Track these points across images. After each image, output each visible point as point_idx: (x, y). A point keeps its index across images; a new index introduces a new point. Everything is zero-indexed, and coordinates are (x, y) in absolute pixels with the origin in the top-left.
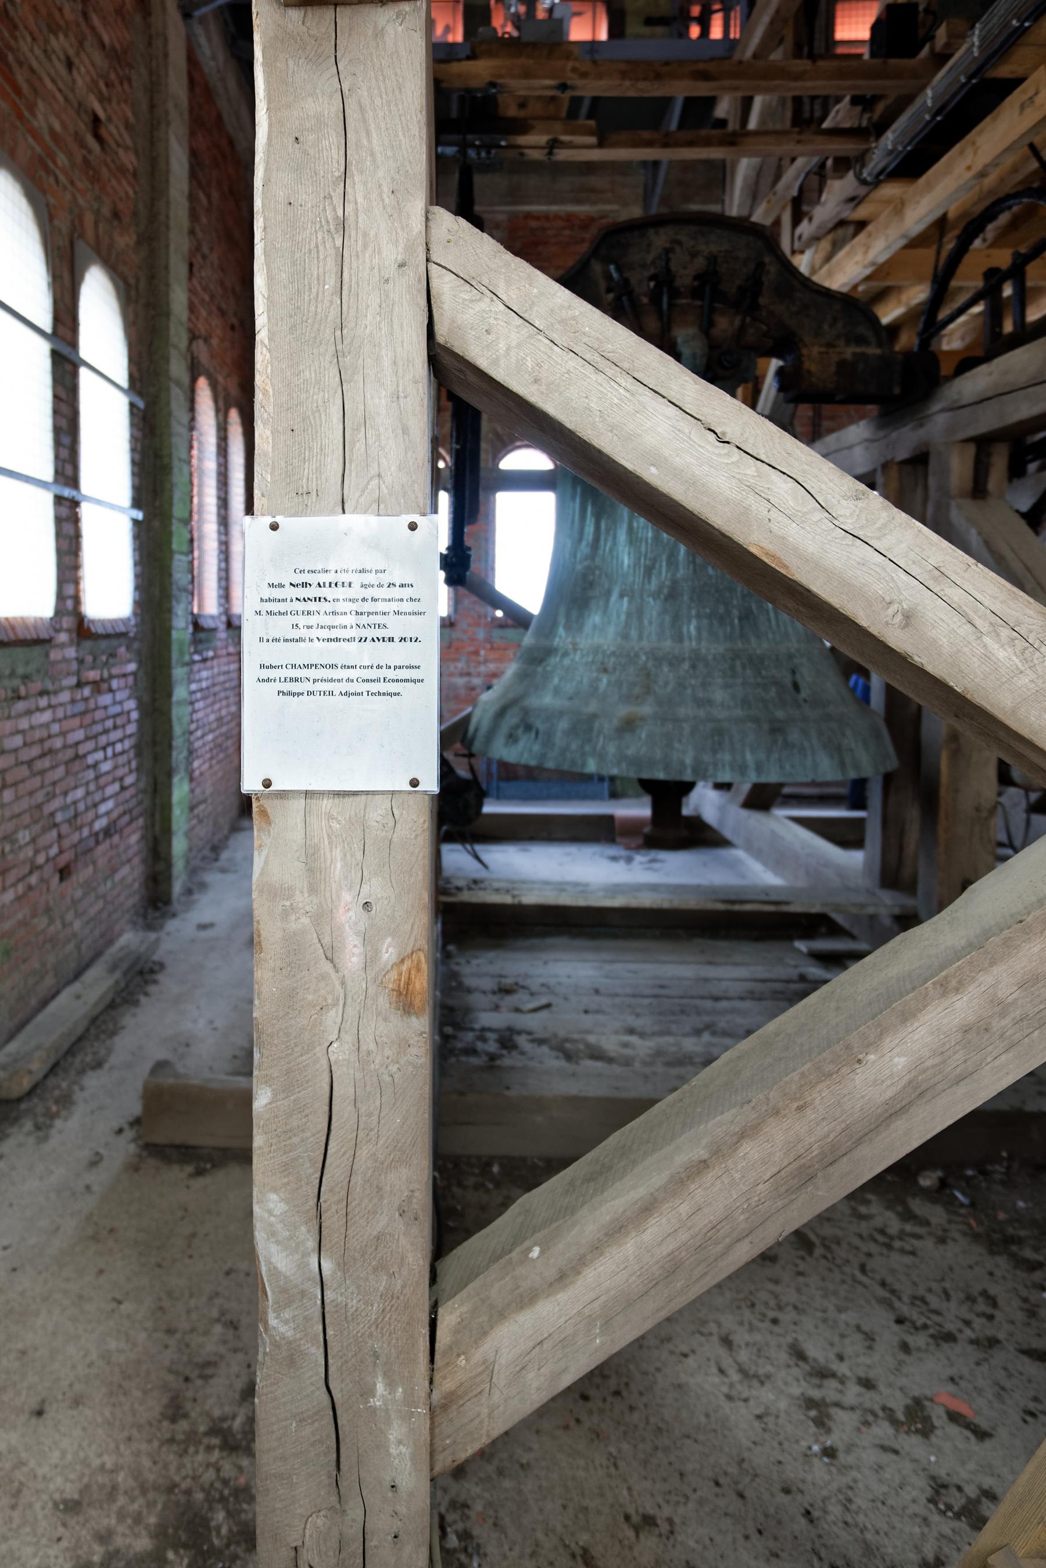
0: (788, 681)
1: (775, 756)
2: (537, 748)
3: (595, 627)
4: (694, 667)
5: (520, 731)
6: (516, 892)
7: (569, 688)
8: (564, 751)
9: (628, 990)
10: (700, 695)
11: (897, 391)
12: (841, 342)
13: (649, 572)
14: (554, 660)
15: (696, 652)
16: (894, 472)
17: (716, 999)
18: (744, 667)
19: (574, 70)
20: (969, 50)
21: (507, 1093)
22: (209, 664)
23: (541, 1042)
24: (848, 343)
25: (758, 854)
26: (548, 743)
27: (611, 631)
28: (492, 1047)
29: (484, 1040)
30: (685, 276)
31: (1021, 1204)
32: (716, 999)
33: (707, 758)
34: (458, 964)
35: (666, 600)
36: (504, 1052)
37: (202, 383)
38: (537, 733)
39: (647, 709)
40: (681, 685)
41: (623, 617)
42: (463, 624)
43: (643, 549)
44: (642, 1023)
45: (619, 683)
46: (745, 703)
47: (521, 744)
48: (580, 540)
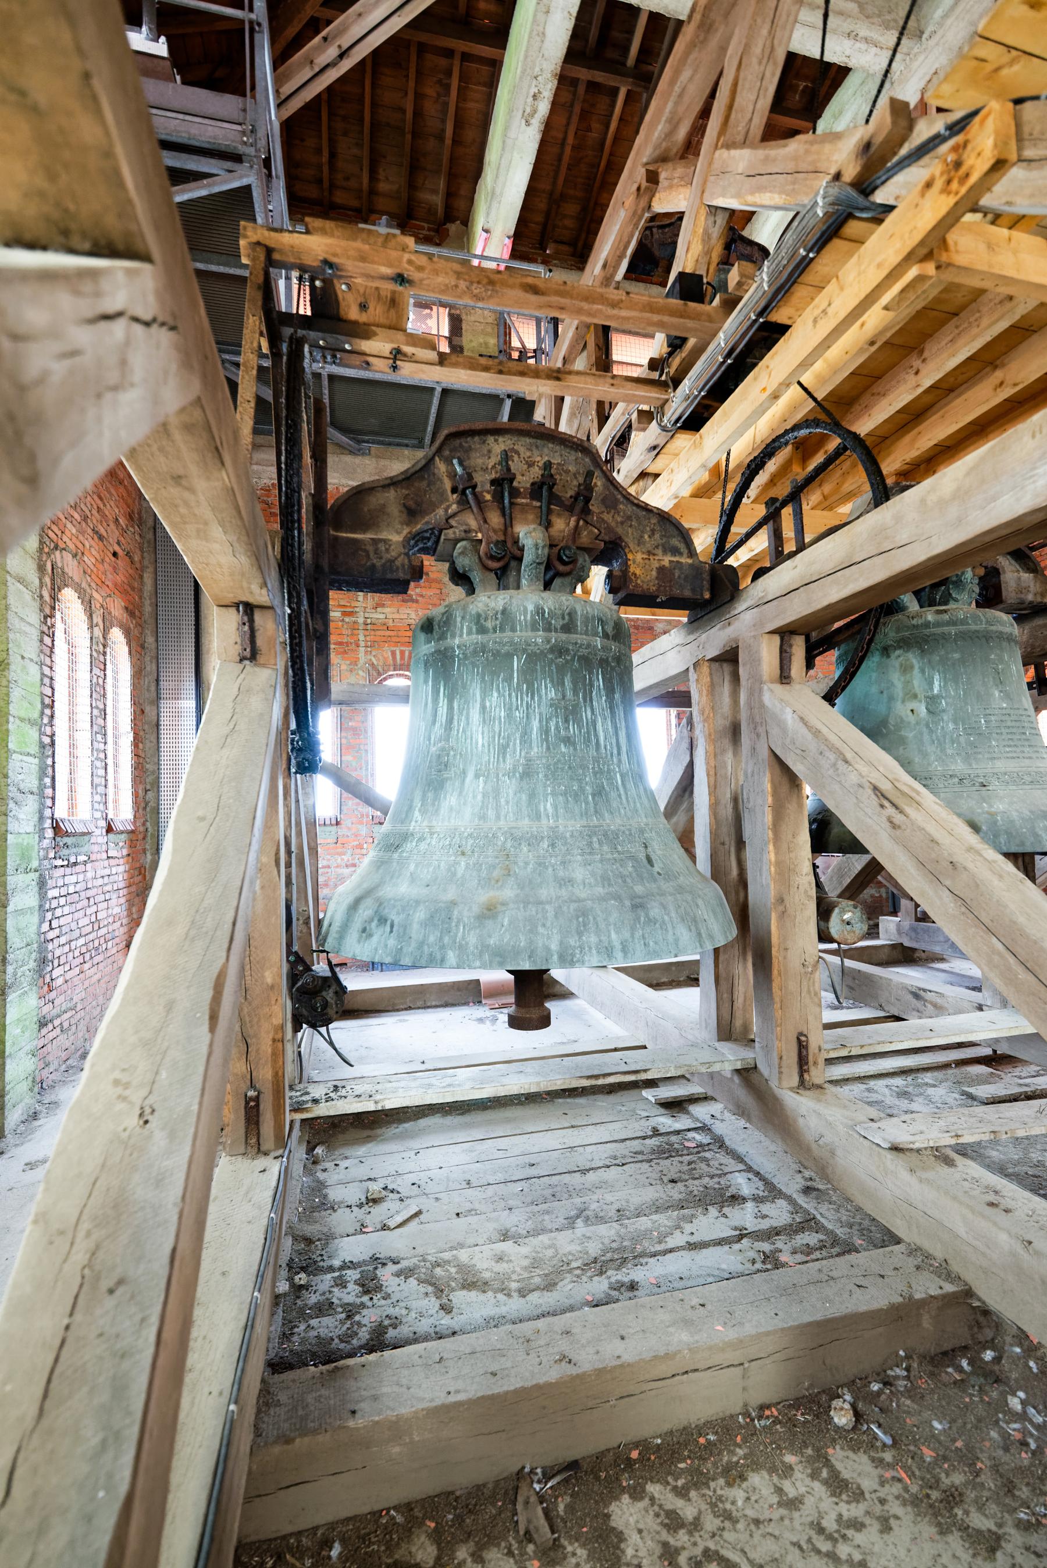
0: (642, 856)
1: (639, 933)
2: (392, 942)
3: (451, 809)
4: (553, 845)
5: (374, 924)
6: (378, 1097)
7: (425, 874)
8: (421, 944)
9: (500, 1177)
10: (561, 874)
11: (707, 595)
12: (659, 551)
13: (503, 750)
14: (409, 846)
15: (554, 829)
16: (705, 669)
17: (584, 1172)
18: (600, 843)
19: (410, 262)
20: (761, 285)
21: (351, 1424)
22: (79, 868)
23: (406, 1273)
24: (665, 552)
25: (601, 1007)
26: (404, 935)
27: (468, 812)
28: (351, 1294)
29: (341, 1283)
30: (524, 480)
31: (937, 1425)
32: (584, 1172)
33: (572, 941)
34: (324, 1170)
35: (521, 778)
36: (365, 1299)
37: (68, 595)
38: (392, 926)
39: (508, 893)
40: (541, 864)
41: (480, 797)
42: (346, 823)
43: (497, 729)
44: (514, 1220)
45: (478, 866)
46: (605, 879)
47: (375, 939)
48: (434, 722)
